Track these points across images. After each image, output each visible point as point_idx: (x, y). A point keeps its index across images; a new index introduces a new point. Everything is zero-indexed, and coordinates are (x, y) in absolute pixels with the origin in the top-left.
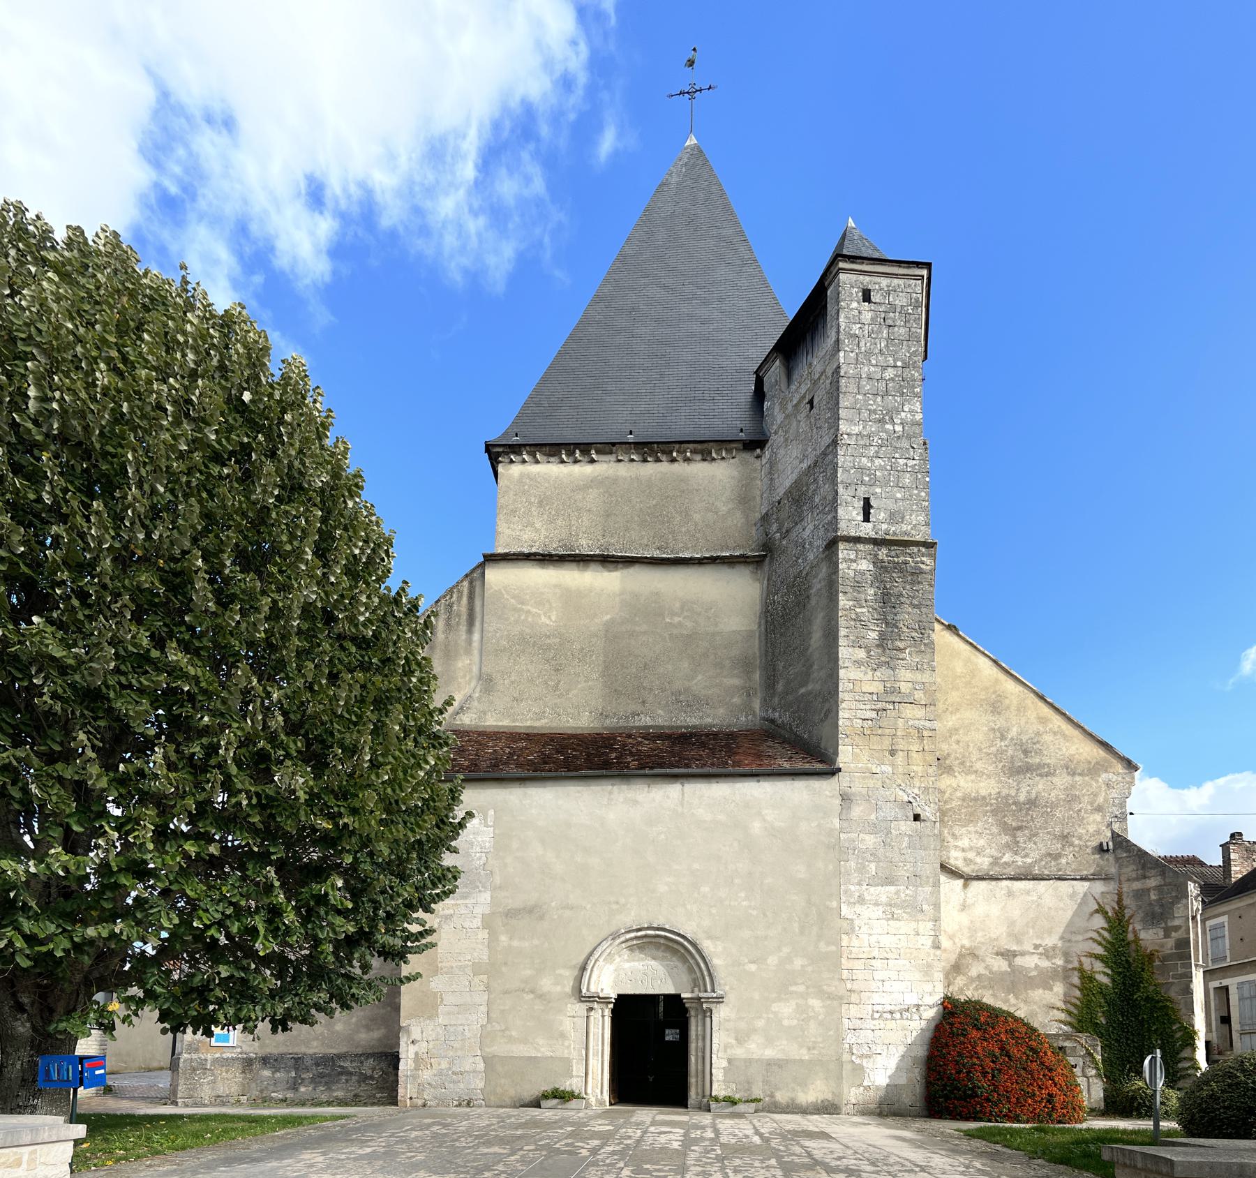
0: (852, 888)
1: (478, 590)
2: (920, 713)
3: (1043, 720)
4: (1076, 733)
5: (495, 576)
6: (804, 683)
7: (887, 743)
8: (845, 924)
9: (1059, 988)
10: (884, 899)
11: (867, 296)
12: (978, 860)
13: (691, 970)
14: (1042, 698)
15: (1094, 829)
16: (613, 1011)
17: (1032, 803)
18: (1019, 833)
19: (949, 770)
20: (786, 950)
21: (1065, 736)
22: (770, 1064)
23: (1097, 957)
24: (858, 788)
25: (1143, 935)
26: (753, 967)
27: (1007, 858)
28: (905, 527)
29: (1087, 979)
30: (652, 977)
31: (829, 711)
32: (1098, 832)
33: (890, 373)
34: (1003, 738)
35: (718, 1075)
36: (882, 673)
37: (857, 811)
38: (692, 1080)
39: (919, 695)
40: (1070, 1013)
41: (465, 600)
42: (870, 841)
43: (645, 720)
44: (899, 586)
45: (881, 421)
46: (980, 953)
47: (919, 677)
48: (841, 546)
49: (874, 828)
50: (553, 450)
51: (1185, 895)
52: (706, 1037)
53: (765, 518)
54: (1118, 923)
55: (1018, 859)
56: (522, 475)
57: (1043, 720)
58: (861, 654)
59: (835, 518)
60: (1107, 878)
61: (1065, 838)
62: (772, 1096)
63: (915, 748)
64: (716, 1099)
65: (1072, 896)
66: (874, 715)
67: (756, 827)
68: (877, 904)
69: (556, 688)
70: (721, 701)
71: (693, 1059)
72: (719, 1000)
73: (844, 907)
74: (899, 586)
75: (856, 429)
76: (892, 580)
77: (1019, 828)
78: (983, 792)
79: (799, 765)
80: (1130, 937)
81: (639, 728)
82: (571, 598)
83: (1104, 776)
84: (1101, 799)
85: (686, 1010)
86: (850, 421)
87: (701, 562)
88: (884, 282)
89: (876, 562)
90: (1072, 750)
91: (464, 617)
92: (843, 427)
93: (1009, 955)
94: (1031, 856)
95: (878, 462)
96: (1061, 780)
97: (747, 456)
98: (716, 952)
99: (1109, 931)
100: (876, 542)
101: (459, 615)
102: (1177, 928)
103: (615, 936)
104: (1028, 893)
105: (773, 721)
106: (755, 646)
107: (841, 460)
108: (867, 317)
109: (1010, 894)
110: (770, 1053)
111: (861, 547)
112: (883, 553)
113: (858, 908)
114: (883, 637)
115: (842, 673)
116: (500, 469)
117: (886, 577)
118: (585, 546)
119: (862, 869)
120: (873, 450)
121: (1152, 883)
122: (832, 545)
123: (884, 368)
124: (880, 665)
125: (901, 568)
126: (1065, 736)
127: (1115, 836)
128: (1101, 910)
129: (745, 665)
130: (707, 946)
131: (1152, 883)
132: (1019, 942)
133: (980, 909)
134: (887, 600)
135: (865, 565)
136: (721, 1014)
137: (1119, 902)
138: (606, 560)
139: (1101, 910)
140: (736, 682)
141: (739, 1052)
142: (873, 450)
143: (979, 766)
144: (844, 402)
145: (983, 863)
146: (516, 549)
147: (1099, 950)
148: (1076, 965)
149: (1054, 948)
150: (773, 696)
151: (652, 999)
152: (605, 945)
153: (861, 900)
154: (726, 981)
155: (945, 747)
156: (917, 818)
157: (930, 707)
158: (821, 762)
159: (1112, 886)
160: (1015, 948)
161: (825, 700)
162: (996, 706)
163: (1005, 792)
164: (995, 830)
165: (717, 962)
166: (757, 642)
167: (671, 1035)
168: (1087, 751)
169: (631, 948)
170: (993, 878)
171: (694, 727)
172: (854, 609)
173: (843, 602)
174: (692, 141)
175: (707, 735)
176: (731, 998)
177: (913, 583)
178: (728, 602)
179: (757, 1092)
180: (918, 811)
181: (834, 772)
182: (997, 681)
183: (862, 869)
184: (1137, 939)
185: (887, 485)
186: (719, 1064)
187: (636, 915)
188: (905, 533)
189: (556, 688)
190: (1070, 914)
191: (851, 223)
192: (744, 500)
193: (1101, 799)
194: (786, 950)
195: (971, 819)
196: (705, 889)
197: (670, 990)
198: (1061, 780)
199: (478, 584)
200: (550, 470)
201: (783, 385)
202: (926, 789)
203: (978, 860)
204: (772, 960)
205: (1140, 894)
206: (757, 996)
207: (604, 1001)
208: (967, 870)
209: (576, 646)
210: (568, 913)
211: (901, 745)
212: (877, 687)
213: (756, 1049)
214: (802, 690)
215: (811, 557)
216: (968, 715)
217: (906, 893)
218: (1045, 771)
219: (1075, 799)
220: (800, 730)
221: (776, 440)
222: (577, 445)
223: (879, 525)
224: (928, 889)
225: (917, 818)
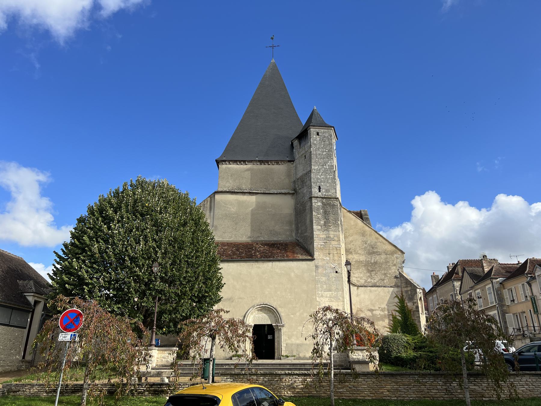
1: (213, 200)
2: (336, 243)
3: (377, 238)
4: (387, 242)
5: (217, 197)
6: (306, 232)
7: (327, 252)
8: (318, 303)
9: (387, 321)
10: (328, 295)
11: (318, 134)
13: (275, 317)
14: (376, 232)
15: (394, 271)
16: (253, 330)
17: (376, 263)
19: (351, 253)
20: (302, 311)
21: (383, 243)
22: (298, 345)
23: (397, 311)
24: (320, 264)
25: (408, 304)
26: (292, 316)
27: (369, 280)
28: (330, 193)
29: (394, 318)
30: (264, 319)
32: (395, 272)
33: (324, 153)
34: (366, 244)
35: (283, 348)
36: (325, 232)
37: (320, 270)
38: (276, 351)
39: (335, 238)
40: (390, 329)
41: (209, 203)
42: (324, 279)
43: (262, 239)
44: (329, 209)
45: (323, 165)
46: (363, 310)
47: (335, 233)
48: (313, 199)
49: (325, 275)
50: (235, 162)
52: (280, 337)
53: (294, 182)
54: (402, 301)
56: (226, 168)
57: (377, 238)
58: (320, 227)
60: (398, 287)
61: (385, 274)
62: (299, 355)
64: (283, 356)
65: (388, 292)
67: (293, 275)
68: (326, 297)
69: (236, 229)
70: (283, 233)
71: (276, 344)
72: (283, 326)
73: (317, 298)
74: (329, 209)
75: (316, 168)
76: (327, 208)
77: (372, 271)
78: (361, 260)
79: (305, 257)
80: (405, 305)
81: (260, 241)
82: (240, 203)
83: (395, 255)
84: (395, 262)
85: (274, 329)
86: (314, 165)
87: (276, 194)
88: (322, 130)
89: (323, 203)
90: (386, 247)
91: (208, 208)
93: (371, 310)
94: (376, 279)
95: (322, 176)
96: (383, 256)
97: (289, 163)
98: (282, 311)
99: (399, 303)
100: (322, 198)
101: (207, 207)
102: (416, 302)
103: (254, 306)
104: (376, 291)
105: (298, 240)
106: (293, 218)
107: (312, 176)
109: (371, 291)
110: (298, 342)
111: (318, 199)
113: (321, 299)
114: (325, 222)
116: (220, 166)
117: (325, 207)
118: (246, 187)
119: (322, 287)
121: (409, 289)
122: (311, 198)
123: (323, 152)
124: (325, 230)
125: (329, 204)
126: (383, 243)
127: (400, 273)
128: (397, 296)
130: (279, 310)
131: (409, 289)
132: (374, 307)
133: (362, 296)
134: (325, 212)
135: (319, 204)
136: (283, 330)
137: (402, 294)
138: (250, 193)
139: (397, 296)
140: (287, 228)
141: (289, 342)
143: (360, 252)
144: (313, 161)
145: (362, 282)
146: (225, 189)
147: (397, 309)
148: (391, 313)
149: (384, 308)
150: (298, 233)
151: (264, 326)
152: (251, 309)
153: (322, 296)
154: (285, 320)
155: (349, 246)
156: (336, 272)
157: (337, 241)
158: (310, 256)
159: (399, 289)
160: (373, 308)
162: (363, 234)
163: (367, 260)
164: (365, 271)
165: (282, 314)
167: (270, 337)
168: (390, 248)
169: (258, 310)
170: (365, 287)
171: (276, 241)
172: (317, 216)
173: (314, 213)
174: (273, 61)
175: (279, 244)
176: (286, 325)
177: (333, 208)
178: (286, 205)
179: (294, 354)
180: (337, 270)
181: (313, 260)
182: (363, 227)
183: (322, 287)
184: (407, 306)
186: (283, 345)
187: (259, 301)
188: (330, 195)
189: (236, 229)
190: (388, 298)
191: (315, 108)
192: (289, 175)
193: (395, 262)
194: (302, 311)
195: (358, 268)
196: (279, 293)
197: (269, 323)
198: (383, 256)
199: (213, 199)
201: (299, 147)
204: (298, 314)
206: (294, 325)
207: (251, 326)
208: (358, 284)
209: (242, 217)
210: (240, 300)
211: (331, 252)
212: (324, 236)
213: (294, 341)
216: (356, 237)
217: (334, 293)
218: (379, 254)
219: (388, 262)
221: (297, 161)
223: (323, 193)
225: (336, 272)
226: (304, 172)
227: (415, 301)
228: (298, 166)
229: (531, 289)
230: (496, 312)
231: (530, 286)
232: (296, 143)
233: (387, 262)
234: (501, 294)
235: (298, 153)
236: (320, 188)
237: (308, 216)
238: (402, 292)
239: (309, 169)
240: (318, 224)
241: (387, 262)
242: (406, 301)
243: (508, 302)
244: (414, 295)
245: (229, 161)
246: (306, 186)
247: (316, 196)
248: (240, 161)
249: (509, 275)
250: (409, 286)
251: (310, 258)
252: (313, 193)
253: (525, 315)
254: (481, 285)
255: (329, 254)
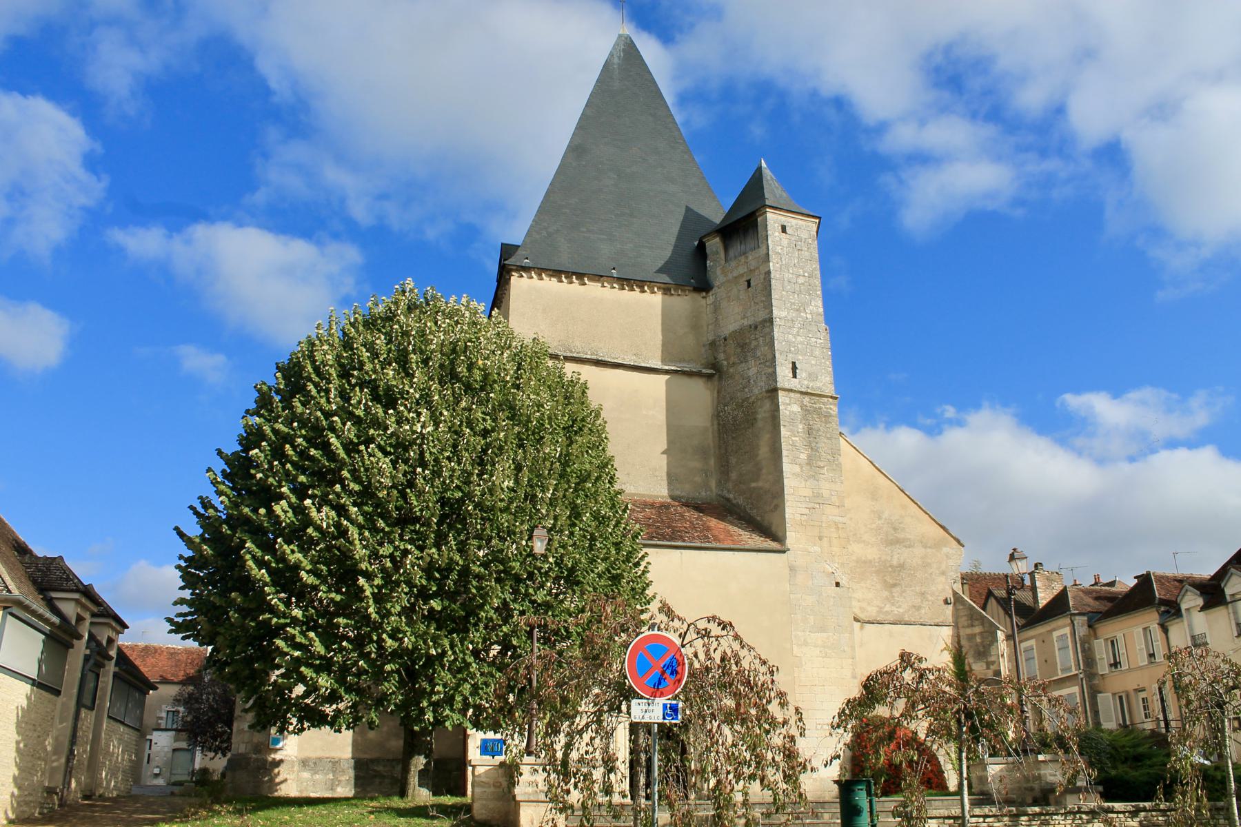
0: (800, 634)
2: (836, 511)
11: (784, 229)
12: (869, 609)
17: (901, 566)
18: (894, 590)
25: (974, 667)
27: (888, 608)
28: (819, 384)
31: (776, 507)
32: (944, 590)
34: (880, 518)
39: (834, 499)
44: (817, 424)
51: (995, 639)
53: (713, 345)
55: (894, 608)
58: (797, 469)
59: (775, 372)
63: (835, 535)
66: (807, 511)
68: (816, 646)
73: (795, 648)
74: (817, 424)
75: (784, 314)
77: (894, 585)
78: (870, 557)
80: (967, 668)
88: (794, 222)
92: (775, 312)
96: (919, 551)
97: (697, 297)
100: (802, 393)
102: (993, 663)
105: (728, 500)
106: (710, 440)
108: (785, 242)
111: (792, 395)
112: (807, 399)
114: (809, 457)
115: (786, 481)
120: (795, 330)
121: (977, 630)
123: (798, 276)
124: (809, 477)
125: (818, 411)
129: (703, 452)
130: (865, 672)
131: (977, 630)
135: (796, 408)
137: (959, 642)
142: (795, 330)
144: (775, 295)
153: (806, 644)
161: (774, 497)
162: (874, 495)
164: (879, 586)
166: (711, 436)
177: (826, 422)
184: (971, 670)
185: (806, 354)
192: (695, 327)
193: (943, 567)
198: (919, 551)
200: (549, 284)
202: (843, 564)
203: (869, 609)
205: (971, 637)
212: (808, 493)
214: (753, 485)
215: (756, 391)
220: (754, 513)
221: (718, 292)
222: (574, 273)
224: (847, 635)
225: (837, 584)
226: (746, 322)
227: (993, 659)
228: (724, 304)
229: (1167, 638)
230: (1075, 689)
231: (1165, 630)
232: (714, 244)
233: (926, 565)
234: (1089, 649)
235: (720, 267)
236: (794, 368)
237: (765, 438)
238: (958, 636)
239: (762, 315)
240: (794, 462)
241: (926, 565)
242: (970, 660)
243: (1103, 667)
244: (990, 645)
245: (541, 271)
246: (756, 358)
247: (787, 386)
248: (569, 274)
249: (1104, 606)
250: (977, 623)
251: (774, 545)
252: (779, 379)
253: (1142, 695)
254: (1041, 630)
255: (820, 538)
